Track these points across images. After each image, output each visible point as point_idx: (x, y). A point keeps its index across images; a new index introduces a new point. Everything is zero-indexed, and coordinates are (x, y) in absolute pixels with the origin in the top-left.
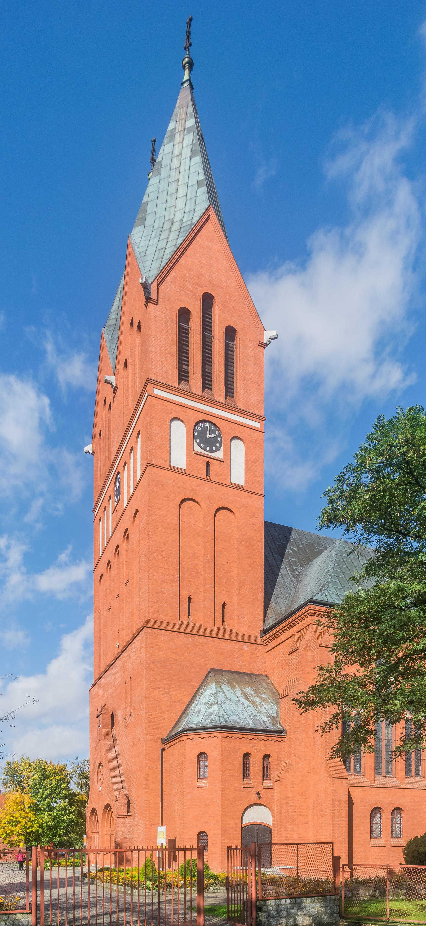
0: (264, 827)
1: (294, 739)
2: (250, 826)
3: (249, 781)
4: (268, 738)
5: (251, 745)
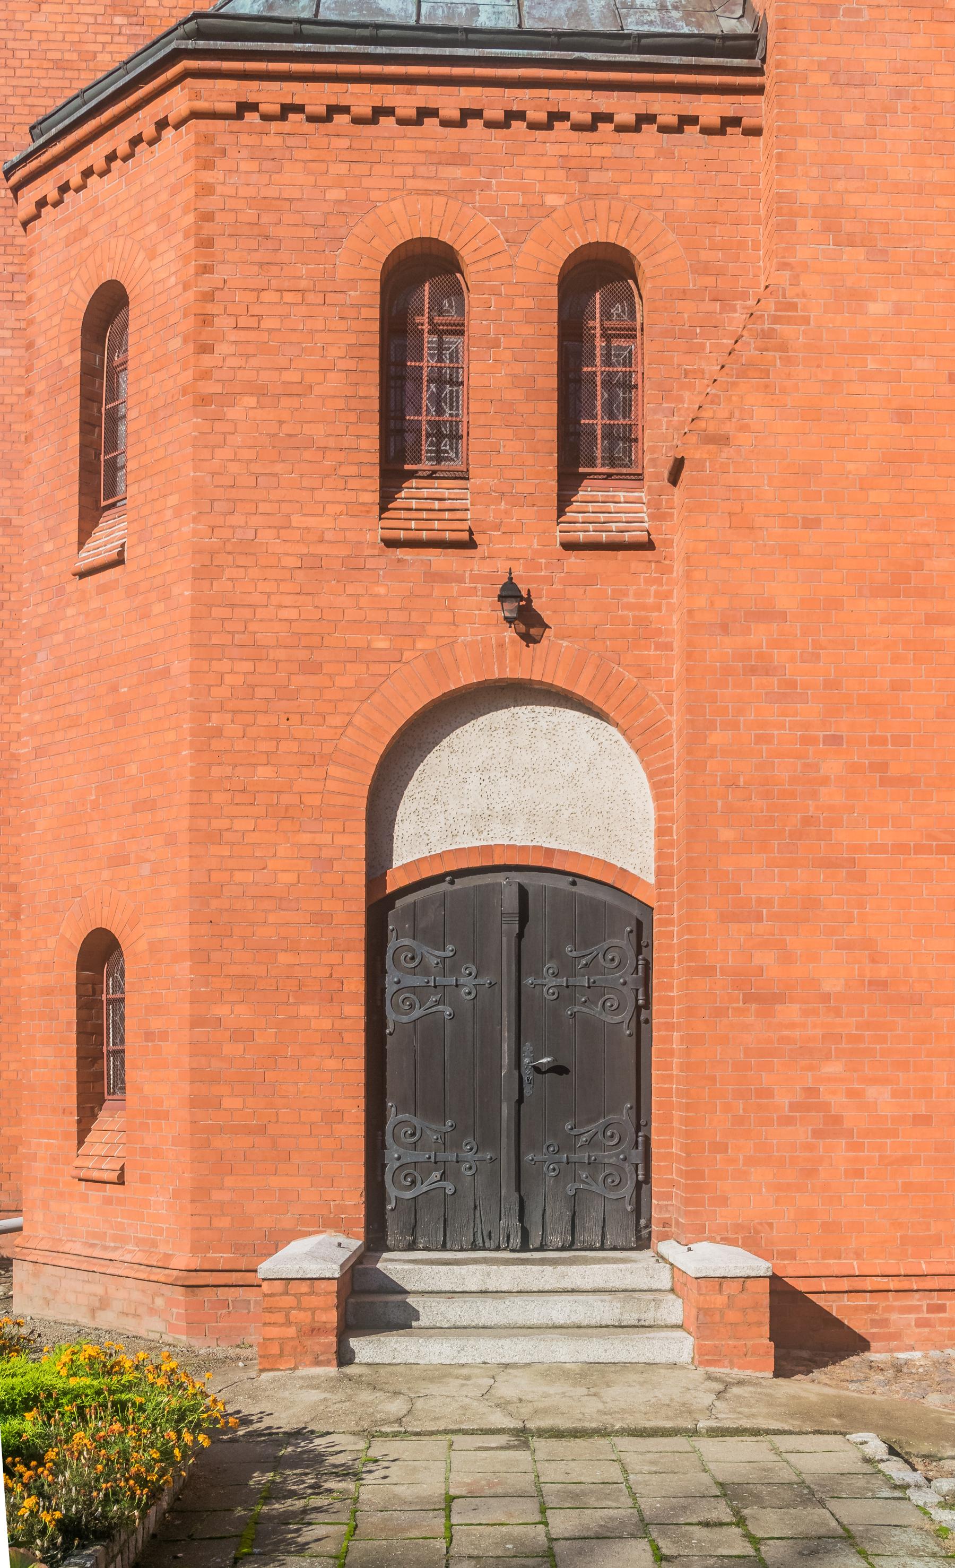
0: (582, 889)
1: (819, 79)
2: (460, 883)
3: (444, 488)
4: (604, 102)
5: (457, 172)
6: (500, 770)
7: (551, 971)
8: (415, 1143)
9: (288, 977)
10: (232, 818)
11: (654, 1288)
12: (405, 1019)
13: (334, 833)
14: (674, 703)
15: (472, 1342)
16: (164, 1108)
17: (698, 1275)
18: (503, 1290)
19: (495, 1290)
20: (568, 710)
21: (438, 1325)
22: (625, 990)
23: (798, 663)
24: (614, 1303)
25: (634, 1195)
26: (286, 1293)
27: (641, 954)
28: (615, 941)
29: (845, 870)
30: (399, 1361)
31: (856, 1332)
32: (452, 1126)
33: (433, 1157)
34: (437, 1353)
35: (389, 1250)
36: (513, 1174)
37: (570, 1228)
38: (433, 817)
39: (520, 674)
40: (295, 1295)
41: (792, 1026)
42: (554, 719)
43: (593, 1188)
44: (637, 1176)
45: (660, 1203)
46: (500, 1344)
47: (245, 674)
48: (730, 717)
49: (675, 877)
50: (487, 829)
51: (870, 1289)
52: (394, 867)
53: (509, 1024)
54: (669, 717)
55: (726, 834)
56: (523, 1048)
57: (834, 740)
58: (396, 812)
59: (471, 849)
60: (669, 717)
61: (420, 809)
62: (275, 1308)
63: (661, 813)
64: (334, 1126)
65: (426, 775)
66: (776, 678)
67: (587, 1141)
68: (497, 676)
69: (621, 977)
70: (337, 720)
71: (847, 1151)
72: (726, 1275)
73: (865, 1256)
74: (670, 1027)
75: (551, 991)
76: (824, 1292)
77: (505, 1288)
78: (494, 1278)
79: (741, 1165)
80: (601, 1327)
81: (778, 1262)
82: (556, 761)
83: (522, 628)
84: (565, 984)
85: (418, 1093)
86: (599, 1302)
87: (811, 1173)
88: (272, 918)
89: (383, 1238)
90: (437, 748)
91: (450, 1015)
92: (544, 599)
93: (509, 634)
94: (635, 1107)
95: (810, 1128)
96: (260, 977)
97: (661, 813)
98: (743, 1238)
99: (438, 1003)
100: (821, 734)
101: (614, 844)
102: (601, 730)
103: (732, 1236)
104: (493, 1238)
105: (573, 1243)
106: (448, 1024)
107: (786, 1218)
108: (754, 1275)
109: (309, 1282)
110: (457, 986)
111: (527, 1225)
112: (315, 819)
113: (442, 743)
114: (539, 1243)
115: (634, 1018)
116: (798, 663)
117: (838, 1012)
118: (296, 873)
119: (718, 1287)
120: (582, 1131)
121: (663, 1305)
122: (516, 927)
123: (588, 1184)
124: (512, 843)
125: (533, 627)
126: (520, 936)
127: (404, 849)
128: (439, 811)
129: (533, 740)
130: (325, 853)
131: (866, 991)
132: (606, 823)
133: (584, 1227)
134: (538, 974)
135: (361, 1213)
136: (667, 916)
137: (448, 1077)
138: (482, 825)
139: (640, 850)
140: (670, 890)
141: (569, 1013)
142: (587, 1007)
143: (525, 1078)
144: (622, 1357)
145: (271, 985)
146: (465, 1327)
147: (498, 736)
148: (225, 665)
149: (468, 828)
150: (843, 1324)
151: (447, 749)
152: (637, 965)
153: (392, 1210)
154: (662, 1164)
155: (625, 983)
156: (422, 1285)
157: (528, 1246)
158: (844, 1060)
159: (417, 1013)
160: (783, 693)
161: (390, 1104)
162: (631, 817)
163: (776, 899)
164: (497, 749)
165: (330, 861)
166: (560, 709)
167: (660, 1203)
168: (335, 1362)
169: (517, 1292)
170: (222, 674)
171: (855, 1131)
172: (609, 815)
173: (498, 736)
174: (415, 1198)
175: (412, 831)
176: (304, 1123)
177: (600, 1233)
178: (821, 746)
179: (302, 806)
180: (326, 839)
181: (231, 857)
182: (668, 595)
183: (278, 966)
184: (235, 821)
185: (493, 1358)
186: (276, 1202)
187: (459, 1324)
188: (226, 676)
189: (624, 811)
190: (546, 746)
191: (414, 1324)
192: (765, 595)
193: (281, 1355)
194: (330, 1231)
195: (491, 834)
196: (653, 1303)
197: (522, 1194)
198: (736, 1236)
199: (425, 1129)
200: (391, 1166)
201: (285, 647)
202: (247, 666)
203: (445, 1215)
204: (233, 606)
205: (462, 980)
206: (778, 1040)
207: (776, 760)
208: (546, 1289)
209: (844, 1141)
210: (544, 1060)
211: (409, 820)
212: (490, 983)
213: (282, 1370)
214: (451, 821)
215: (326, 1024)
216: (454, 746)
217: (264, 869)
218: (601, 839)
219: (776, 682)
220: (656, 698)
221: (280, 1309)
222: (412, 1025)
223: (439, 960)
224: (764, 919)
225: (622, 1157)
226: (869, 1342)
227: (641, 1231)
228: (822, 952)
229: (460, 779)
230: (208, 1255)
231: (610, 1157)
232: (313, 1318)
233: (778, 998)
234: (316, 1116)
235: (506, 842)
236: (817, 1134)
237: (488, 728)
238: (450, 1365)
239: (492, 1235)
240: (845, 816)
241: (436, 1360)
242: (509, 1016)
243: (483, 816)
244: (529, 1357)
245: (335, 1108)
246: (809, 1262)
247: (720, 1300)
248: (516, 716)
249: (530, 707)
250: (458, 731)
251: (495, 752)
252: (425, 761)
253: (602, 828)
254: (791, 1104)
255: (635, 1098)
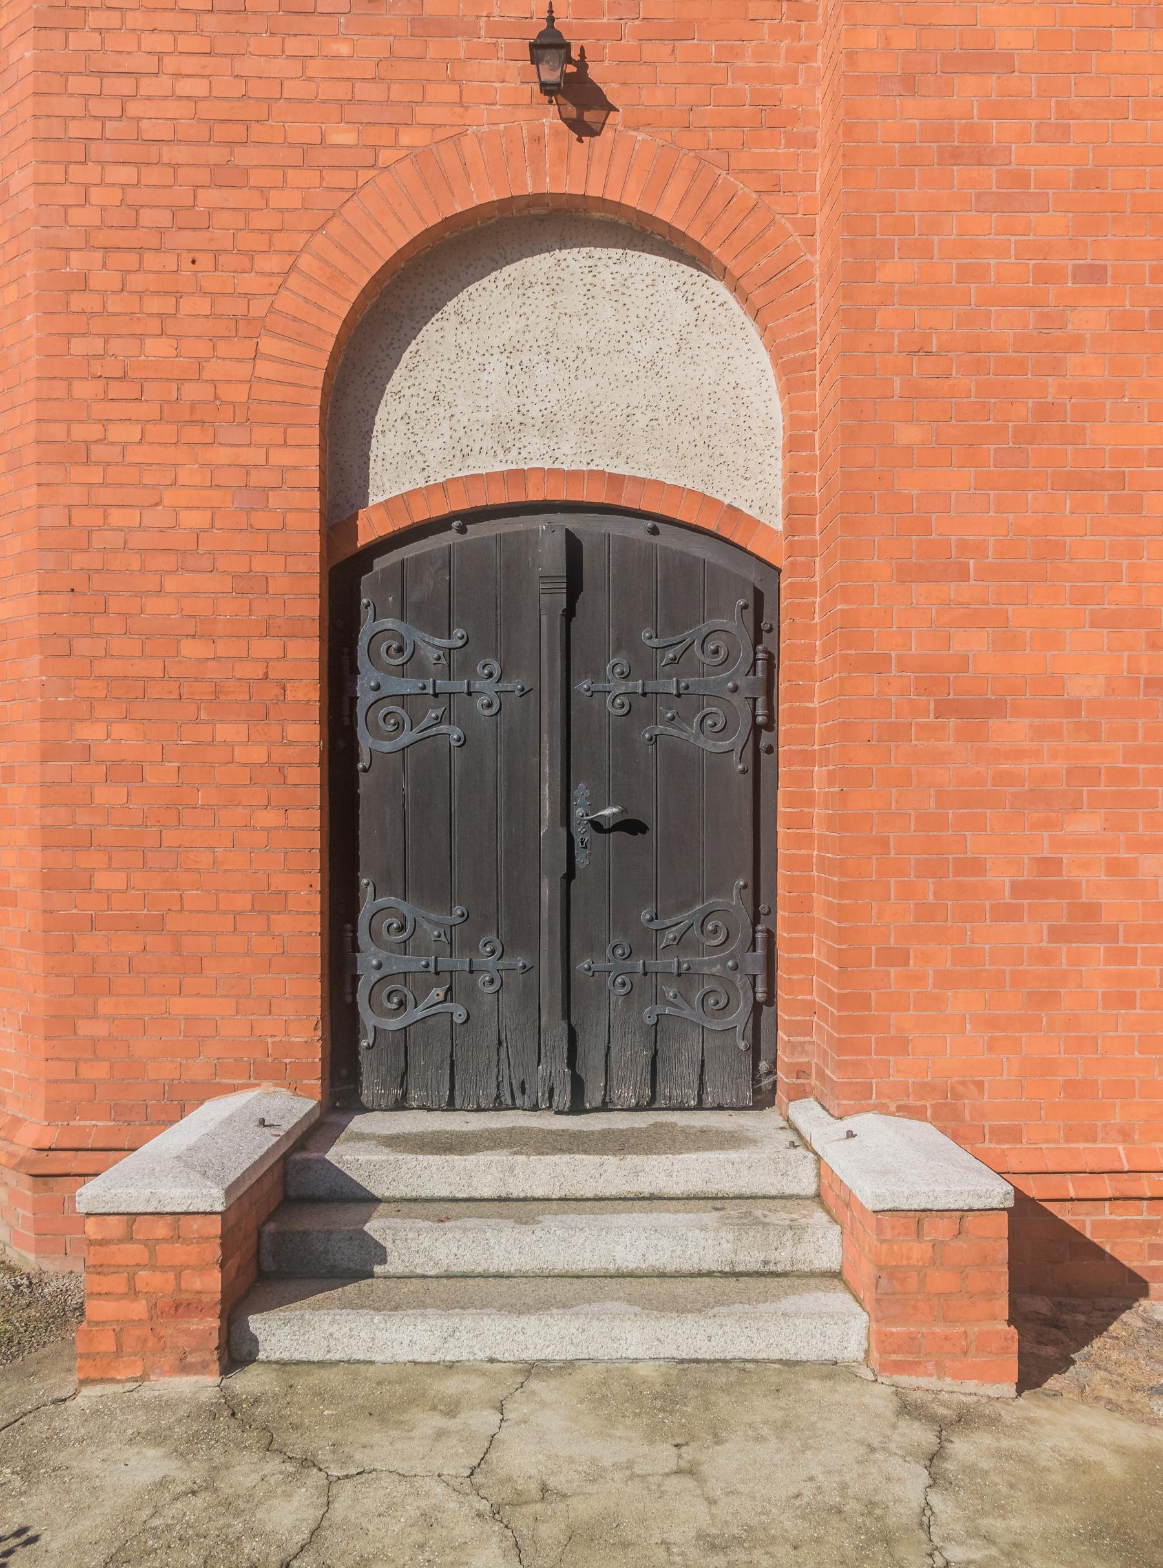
0: (668, 539)
2: (477, 531)
6: (538, 350)
7: (618, 670)
8: (405, 942)
9: (197, 680)
10: (106, 422)
11: (788, 1192)
12: (387, 746)
13: (269, 446)
14: (817, 234)
15: (468, 1322)
16: (11, 888)
17: (879, 1207)
18: (536, 1196)
19: (522, 1195)
20: (646, 255)
21: (419, 1271)
22: (736, 699)
23: (1033, 144)
24: (723, 1234)
25: (750, 1025)
26: (130, 1238)
27: (761, 643)
28: (718, 622)
29: (1106, 493)
30: (337, 1357)
31: (1123, 1266)
32: (463, 915)
33: (432, 964)
34: (406, 1342)
35: (365, 1110)
36: (559, 994)
37: (649, 1077)
38: (431, 427)
39: (569, 186)
40: (146, 1243)
41: (1017, 755)
42: (623, 269)
43: (686, 1013)
44: (755, 993)
45: (792, 1039)
46: (520, 1326)
47: (124, 187)
48: (917, 236)
49: (818, 517)
50: (518, 445)
51: (1149, 1195)
52: (371, 503)
53: (551, 755)
54: (808, 257)
55: (907, 434)
56: (575, 793)
57: (1093, 274)
58: (373, 418)
59: (490, 476)
60: (808, 257)
61: (411, 413)
62: (109, 1266)
63: (794, 412)
64: (272, 917)
65: (421, 359)
66: (994, 169)
67: (675, 938)
68: (530, 190)
69: (729, 679)
70: (273, 263)
71: (1107, 963)
72: (929, 1206)
73: (1136, 1137)
74: (808, 758)
75: (618, 701)
76: (1072, 1200)
77: (539, 1193)
78: (521, 1176)
79: (930, 987)
80: (700, 1274)
81: (992, 1146)
82: (627, 336)
83: (572, 111)
84: (640, 691)
85: (409, 862)
86: (697, 1232)
87: (1047, 999)
88: (170, 584)
89: (356, 1092)
90: (438, 315)
91: (459, 740)
92: (606, 63)
93: (550, 119)
94: (750, 886)
95: (1045, 925)
96: (153, 679)
97: (794, 412)
98: (934, 1106)
99: (439, 721)
100: (1070, 264)
101: (719, 468)
102: (699, 285)
103: (912, 1102)
104: (527, 1091)
105: (653, 1099)
106: (456, 752)
107: (1005, 1072)
108: (981, 1206)
109: (169, 1218)
110: (469, 693)
111: (581, 1072)
112: (239, 424)
113: (445, 308)
114: (600, 1100)
115: (750, 744)
116: (1033, 144)
117: (1093, 732)
118: (209, 513)
119: (914, 1228)
120: (668, 922)
121: (806, 1237)
122: (562, 599)
123: (677, 1006)
124: (557, 465)
125: (589, 109)
126: (569, 613)
127: (385, 479)
128: (441, 416)
129: (591, 303)
130: (255, 479)
131: (1141, 697)
132: (705, 435)
133: (671, 1074)
134: (597, 674)
135: (316, 1056)
136: (804, 580)
137: (456, 838)
138: (510, 437)
139: (760, 477)
140: (809, 537)
141: (647, 736)
142: (675, 727)
143: (578, 840)
144: (739, 1349)
145: (171, 692)
146: (465, 1276)
147: (534, 296)
148: (91, 173)
149: (487, 444)
150: (1103, 1252)
151: (453, 318)
152: (755, 660)
153: (369, 1048)
154: (795, 977)
155: (735, 689)
156: (401, 1187)
157: (583, 1103)
158: (1103, 811)
159: (407, 737)
160: (1007, 194)
161: (365, 881)
162: (745, 426)
163: (991, 543)
164: (533, 318)
165: (265, 490)
166: (633, 253)
167: (792, 1039)
168: (216, 1367)
169: (559, 1199)
170: (87, 186)
171: (1121, 929)
172: (710, 422)
173: (534, 296)
174: (405, 1028)
175: (398, 449)
176: (224, 913)
177: (696, 1085)
178: (1070, 284)
179: (218, 402)
180: (255, 456)
181: (104, 484)
182: (807, 56)
183: (180, 662)
184: (111, 427)
185: (508, 1351)
186: (181, 1038)
187: (454, 1269)
188: (93, 190)
189: (734, 415)
190: (610, 312)
191: (378, 1269)
192: (979, 27)
193: (119, 1352)
194: (267, 1086)
195: (524, 453)
196: (790, 1234)
197: (573, 1023)
198: (923, 1102)
199: (419, 920)
200: (367, 977)
201: (188, 142)
202: (126, 174)
203: (451, 1056)
204: (101, 74)
205: (477, 685)
206: (994, 778)
207: (993, 309)
208: (608, 1195)
209: (1102, 947)
210: (608, 812)
211: (393, 431)
212: (523, 689)
213: (119, 1381)
214: (461, 432)
215: (258, 754)
216: (464, 312)
217: (156, 505)
218: (697, 460)
219: (994, 177)
220: (788, 225)
221: (117, 1268)
222: (399, 756)
223: (441, 653)
224: (972, 576)
225: (730, 963)
226: (1146, 1282)
227: (760, 1081)
228: (1068, 631)
229: (475, 365)
230: (73, 1123)
231: (711, 965)
232: (178, 1285)
233: (995, 708)
234: (243, 902)
235: (547, 465)
236: (1056, 934)
237: (518, 283)
238: (429, 1363)
239: (527, 1086)
240: (1108, 402)
241: (404, 1355)
242: (551, 742)
243: (511, 424)
244: (572, 1349)
245: (273, 889)
246: (1044, 1146)
247: (918, 1251)
248: (563, 264)
249: (584, 250)
250: (471, 288)
251: (529, 322)
252: (419, 337)
253: (700, 443)
254: (1014, 885)
255: (751, 870)
